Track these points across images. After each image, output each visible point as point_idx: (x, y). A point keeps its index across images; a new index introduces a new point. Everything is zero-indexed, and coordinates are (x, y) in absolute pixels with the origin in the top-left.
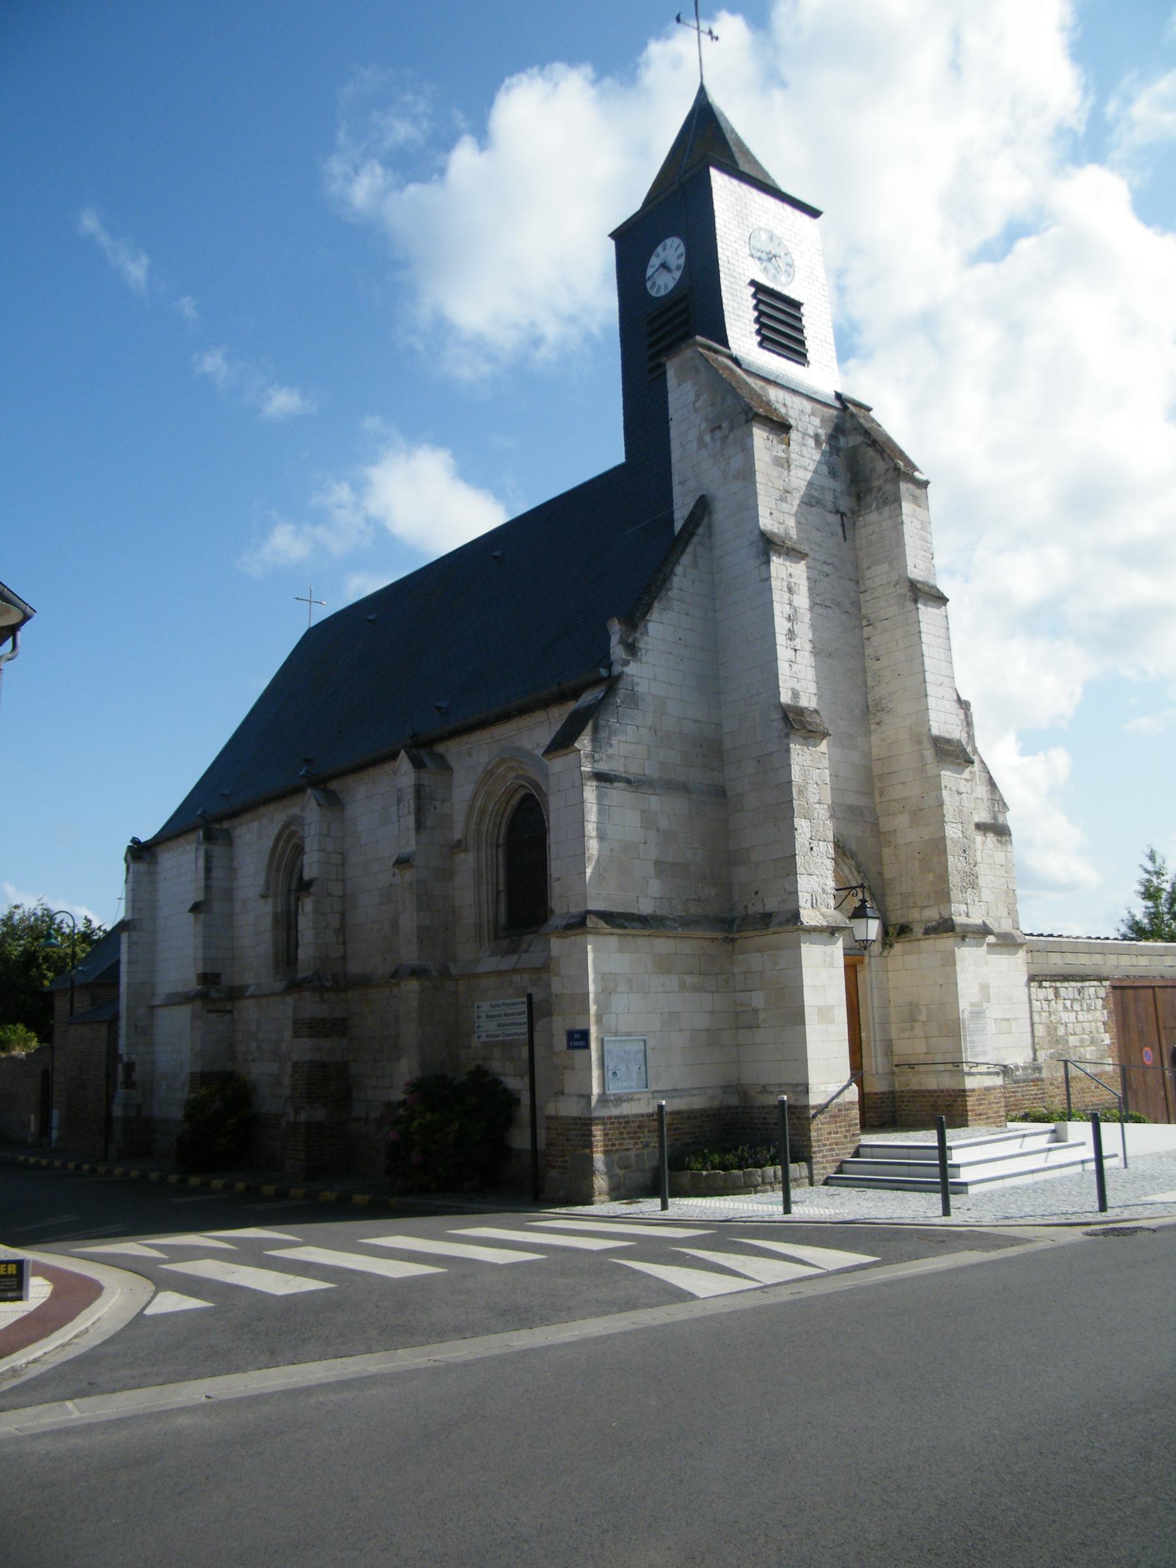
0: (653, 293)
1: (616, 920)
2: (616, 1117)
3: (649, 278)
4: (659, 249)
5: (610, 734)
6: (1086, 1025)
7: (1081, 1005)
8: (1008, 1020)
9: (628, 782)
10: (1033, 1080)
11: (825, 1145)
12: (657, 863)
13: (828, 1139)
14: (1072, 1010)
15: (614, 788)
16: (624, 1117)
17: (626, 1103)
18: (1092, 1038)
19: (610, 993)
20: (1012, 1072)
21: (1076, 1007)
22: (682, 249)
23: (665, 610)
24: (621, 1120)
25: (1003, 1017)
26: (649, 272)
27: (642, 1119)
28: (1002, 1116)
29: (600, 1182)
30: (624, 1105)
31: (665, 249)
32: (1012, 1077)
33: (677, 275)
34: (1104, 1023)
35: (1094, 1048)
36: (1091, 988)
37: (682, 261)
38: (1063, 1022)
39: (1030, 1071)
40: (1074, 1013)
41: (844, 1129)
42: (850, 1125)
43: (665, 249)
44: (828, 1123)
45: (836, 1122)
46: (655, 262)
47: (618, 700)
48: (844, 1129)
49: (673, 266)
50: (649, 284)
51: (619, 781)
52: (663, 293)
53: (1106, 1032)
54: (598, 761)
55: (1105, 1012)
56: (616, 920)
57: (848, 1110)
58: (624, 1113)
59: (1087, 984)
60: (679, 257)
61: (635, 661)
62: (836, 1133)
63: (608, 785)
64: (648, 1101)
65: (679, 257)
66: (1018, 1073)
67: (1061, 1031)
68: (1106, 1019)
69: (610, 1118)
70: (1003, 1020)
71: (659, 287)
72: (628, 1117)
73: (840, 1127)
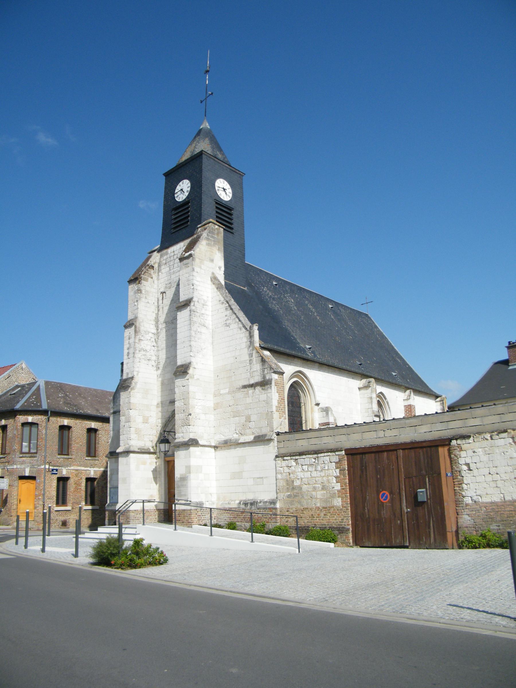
0: (177, 199)
3: (176, 193)
4: (181, 183)
6: (317, 479)
8: (262, 478)
10: (270, 509)
14: (308, 471)
18: (323, 486)
20: (257, 504)
21: (310, 469)
22: (189, 185)
25: (258, 477)
26: (176, 191)
30: (113, 506)
31: (183, 184)
32: (257, 506)
33: (187, 194)
34: (336, 477)
35: (325, 492)
36: (325, 458)
37: (189, 189)
38: (299, 477)
39: (268, 504)
40: (309, 473)
41: (125, 519)
43: (183, 184)
46: (178, 188)
48: (125, 519)
49: (185, 191)
50: (176, 196)
52: (181, 200)
53: (337, 482)
55: (338, 470)
59: (319, 455)
60: (188, 187)
62: (123, 520)
65: (188, 187)
66: (260, 504)
67: (297, 483)
68: (338, 474)
70: (258, 478)
71: (180, 198)
73: (124, 518)
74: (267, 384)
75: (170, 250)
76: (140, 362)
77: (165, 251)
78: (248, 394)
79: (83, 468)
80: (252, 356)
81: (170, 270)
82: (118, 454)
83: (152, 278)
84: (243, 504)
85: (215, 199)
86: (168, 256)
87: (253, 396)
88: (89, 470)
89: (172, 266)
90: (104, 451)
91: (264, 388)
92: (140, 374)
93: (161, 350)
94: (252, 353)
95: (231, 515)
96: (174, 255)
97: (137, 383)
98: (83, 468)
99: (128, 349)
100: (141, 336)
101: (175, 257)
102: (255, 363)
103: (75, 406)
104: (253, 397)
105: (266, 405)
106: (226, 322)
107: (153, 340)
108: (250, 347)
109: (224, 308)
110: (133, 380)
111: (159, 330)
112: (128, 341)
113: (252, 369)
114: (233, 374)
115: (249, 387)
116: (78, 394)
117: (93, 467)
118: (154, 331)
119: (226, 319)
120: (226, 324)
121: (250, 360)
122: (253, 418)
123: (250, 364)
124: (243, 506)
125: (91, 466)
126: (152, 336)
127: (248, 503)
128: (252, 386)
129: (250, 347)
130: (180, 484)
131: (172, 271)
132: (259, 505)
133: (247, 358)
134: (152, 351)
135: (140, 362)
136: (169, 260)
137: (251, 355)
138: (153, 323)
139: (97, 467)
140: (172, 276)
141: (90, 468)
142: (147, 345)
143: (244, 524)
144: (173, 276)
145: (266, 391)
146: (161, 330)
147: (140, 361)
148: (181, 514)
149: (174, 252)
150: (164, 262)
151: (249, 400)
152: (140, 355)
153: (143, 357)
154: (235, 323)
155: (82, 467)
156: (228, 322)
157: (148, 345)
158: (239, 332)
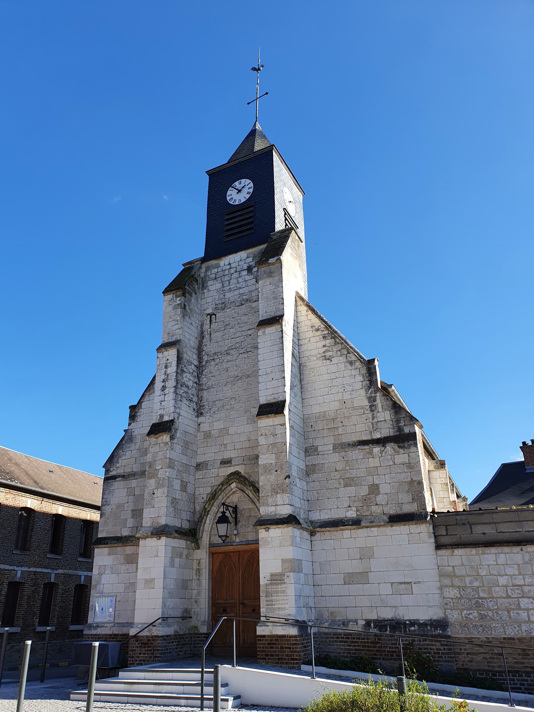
1: (448, 586)
2: (94, 635)
5: (118, 458)
7: (318, 532)
9: (123, 476)
11: (137, 660)
12: (133, 511)
13: (138, 657)
15: (116, 481)
16: (98, 635)
17: (100, 628)
19: (102, 575)
20: (405, 627)
23: (151, 394)
24: (149, 652)
27: (106, 637)
28: (71, 610)
29: (5, 636)
30: (99, 629)
42: (154, 650)
44: (141, 647)
45: (145, 647)
47: (124, 442)
51: (120, 477)
54: (112, 471)
56: (448, 586)
57: (153, 640)
58: (98, 633)
61: (133, 422)
62: (145, 654)
63: (113, 481)
64: (110, 628)
69: (91, 635)
72: (100, 635)
73: (148, 650)
74: (408, 440)
75: (224, 261)
76: (181, 401)
77: (213, 262)
78: (371, 453)
79: (7, 567)
80: (375, 400)
81: (223, 287)
82: (138, 539)
83: (196, 294)
84: (375, 627)
85: (285, 209)
86: (220, 269)
87: (382, 456)
88: (15, 570)
89: (227, 282)
90: (38, 541)
91: (402, 445)
92: (181, 417)
93: (206, 390)
94: (376, 397)
95: (350, 646)
96: (231, 268)
97: (177, 430)
98: (7, 567)
99: (164, 381)
100: (183, 366)
101: (232, 271)
102: (380, 410)
103: (8, 473)
104: (381, 458)
105: (407, 471)
106: (324, 355)
107: (196, 374)
108: (369, 388)
109: (321, 337)
110: (173, 424)
111: (204, 363)
112: (164, 370)
113: (375, 418)
114: (341, 424)
115: (372, 444)
116: (8, 459)
117: (22, 566)
118: (196, 363)
119: (324, 351)
120: (325, 356)
121: (371, 406)
122: (384, 488)
123: (372, 411)
124: (374, 630)
125: (19, 564)
126: (195, 369)
127: (386, 625)
128: (382, 442)
129: (369, 388)
130: (271, 589)
131: (228, 288)
132: (409, 630)
133: (366, 403)
134: (194, 389)
135: (181, 401)
136: (221, 274)
137: (372, 400)
138: (196, 353)
139: (27, 566)
140: (226, 294)
141: (17, 566)
142: (189, 379)
143: (380, 663)
144: (228, 295)
145: (406, 451)
146: (206, 363)
147: (182, 399)
148: (275, 644)
149: (229, 264)
150: (214, 276)
151: (373, 462)
152: (182, 391)
153: (184, 395)
154: (341, 356)
155: (7, 564)
156: (328, 354)
157: (191, 380)
158: (350, 368)
